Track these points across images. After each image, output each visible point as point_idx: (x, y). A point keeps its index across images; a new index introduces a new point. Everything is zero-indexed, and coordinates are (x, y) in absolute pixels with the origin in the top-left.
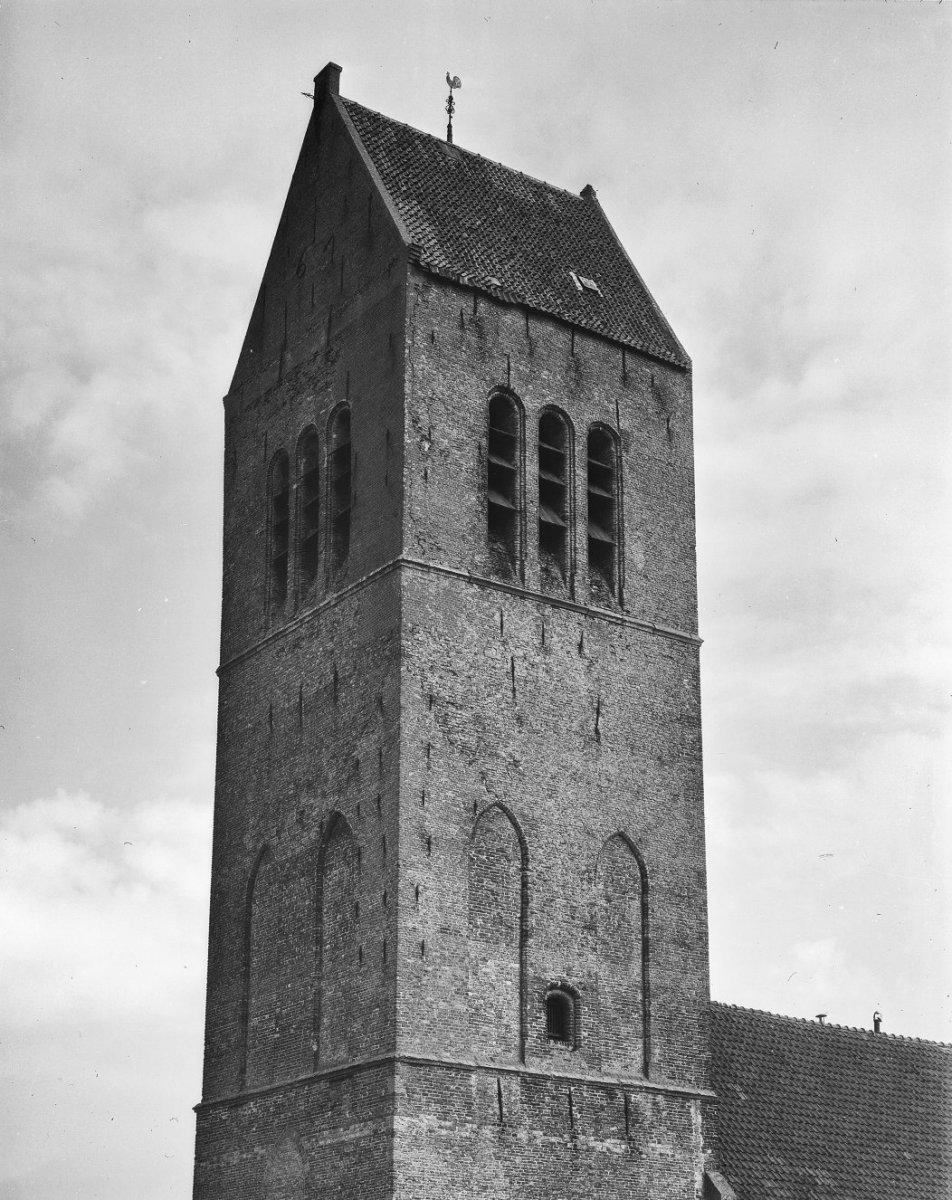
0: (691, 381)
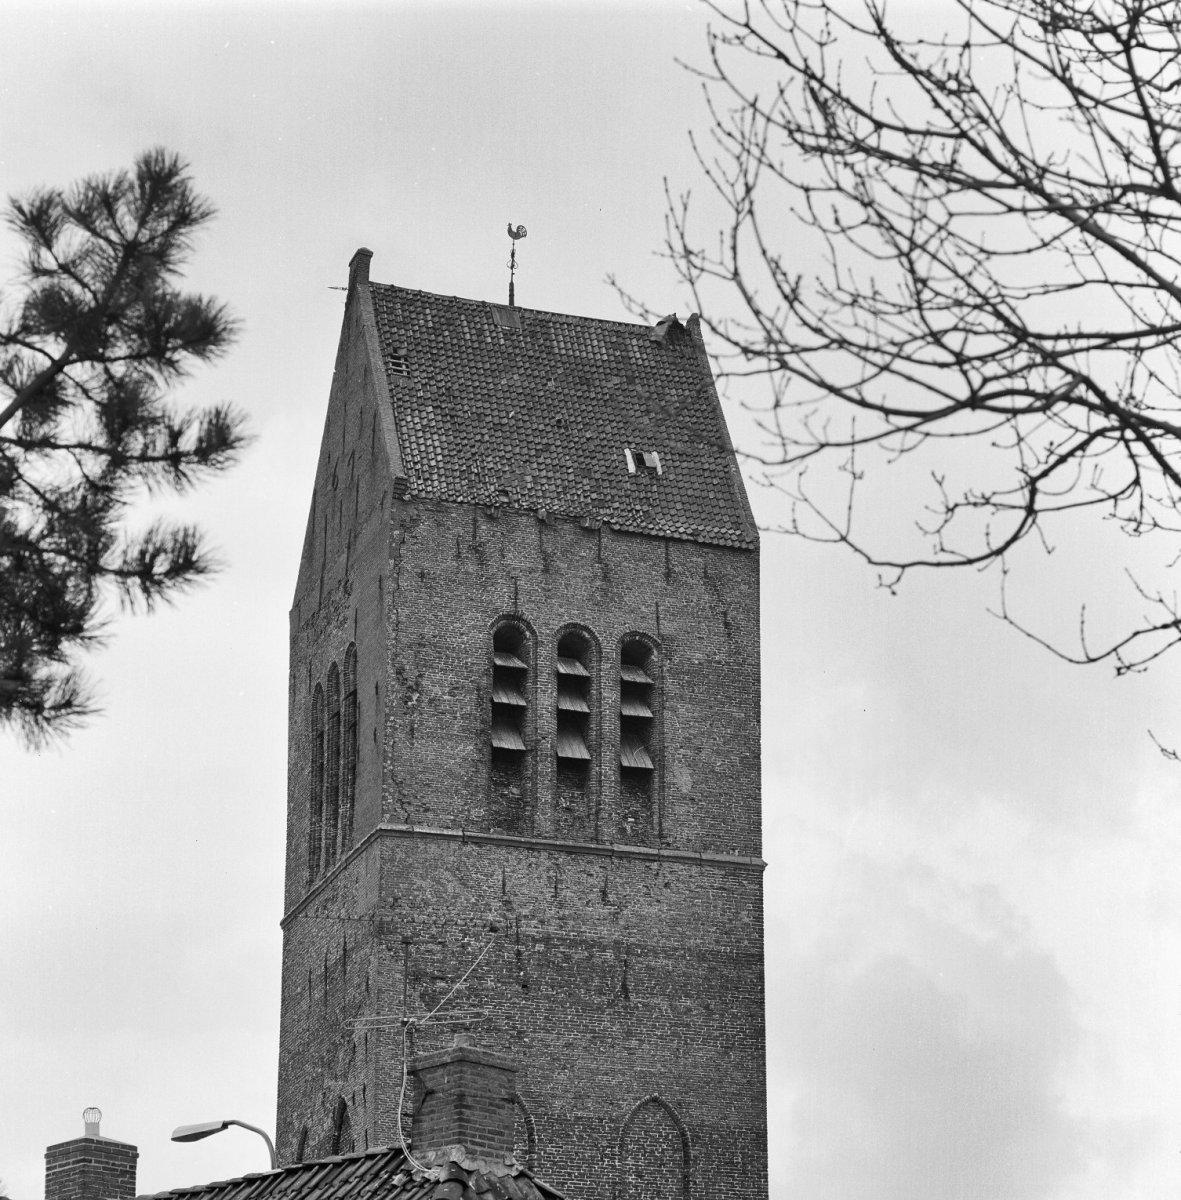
0: (758, 561)
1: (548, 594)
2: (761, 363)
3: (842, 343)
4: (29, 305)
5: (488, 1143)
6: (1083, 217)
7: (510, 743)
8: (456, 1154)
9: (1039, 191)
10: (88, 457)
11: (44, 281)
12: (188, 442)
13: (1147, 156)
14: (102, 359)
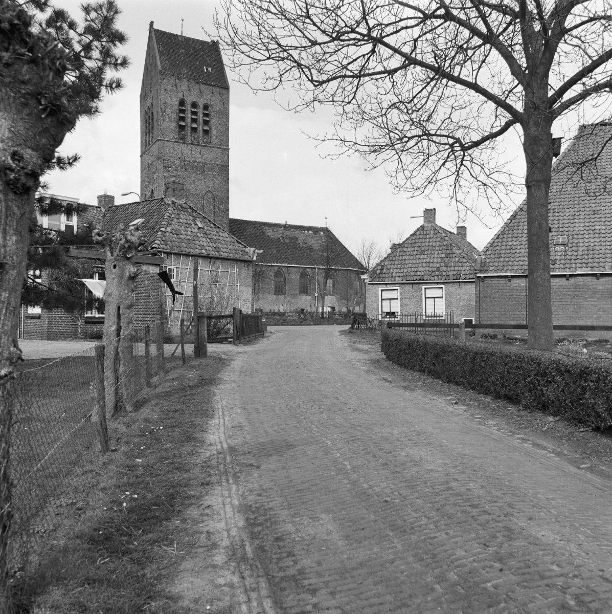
1: (190, 95)
2: (231, 47)
3: (246, 44)
4: (85, 28)
5: (180, 197)
6: (292, 22)
7: (182, 123)
8: (173, 199)
9: (285, 16)
10: (98, 62)
11: (88, 22)
12: (119, 61)
13: (305, 11)
14: (101, 41)
